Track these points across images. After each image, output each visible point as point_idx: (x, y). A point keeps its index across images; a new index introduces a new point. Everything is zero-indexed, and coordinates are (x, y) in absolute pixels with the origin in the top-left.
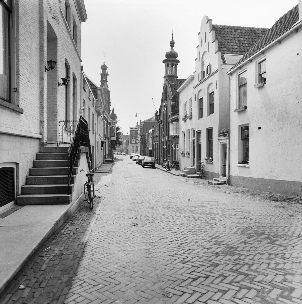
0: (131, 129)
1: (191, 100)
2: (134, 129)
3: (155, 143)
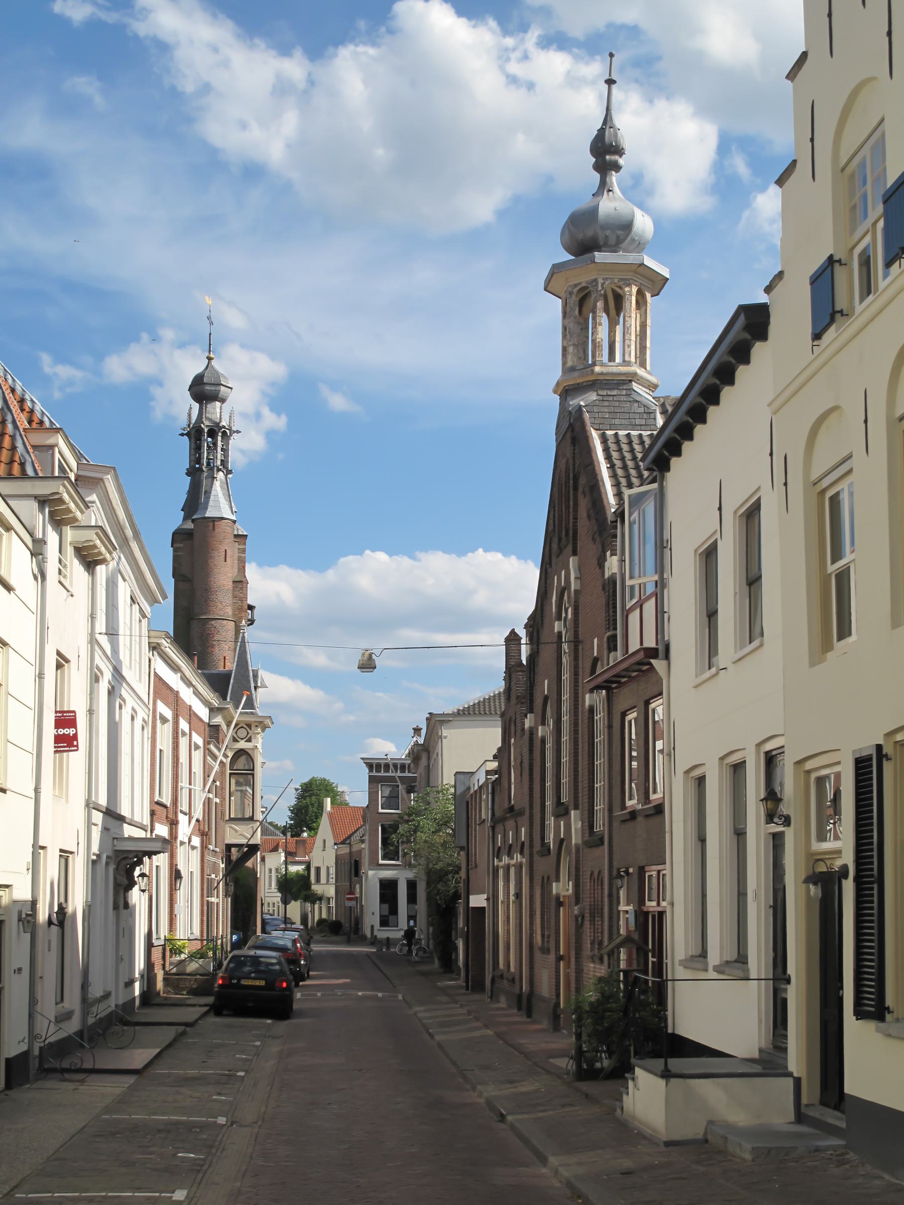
0: (378, 766)
1: (751, 515)
2: (387, 767)
3: (505, 860)
